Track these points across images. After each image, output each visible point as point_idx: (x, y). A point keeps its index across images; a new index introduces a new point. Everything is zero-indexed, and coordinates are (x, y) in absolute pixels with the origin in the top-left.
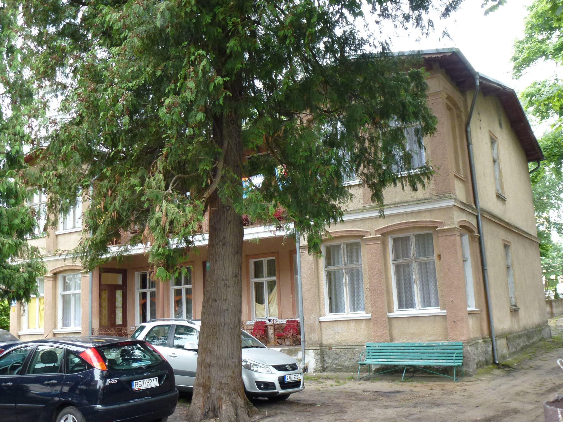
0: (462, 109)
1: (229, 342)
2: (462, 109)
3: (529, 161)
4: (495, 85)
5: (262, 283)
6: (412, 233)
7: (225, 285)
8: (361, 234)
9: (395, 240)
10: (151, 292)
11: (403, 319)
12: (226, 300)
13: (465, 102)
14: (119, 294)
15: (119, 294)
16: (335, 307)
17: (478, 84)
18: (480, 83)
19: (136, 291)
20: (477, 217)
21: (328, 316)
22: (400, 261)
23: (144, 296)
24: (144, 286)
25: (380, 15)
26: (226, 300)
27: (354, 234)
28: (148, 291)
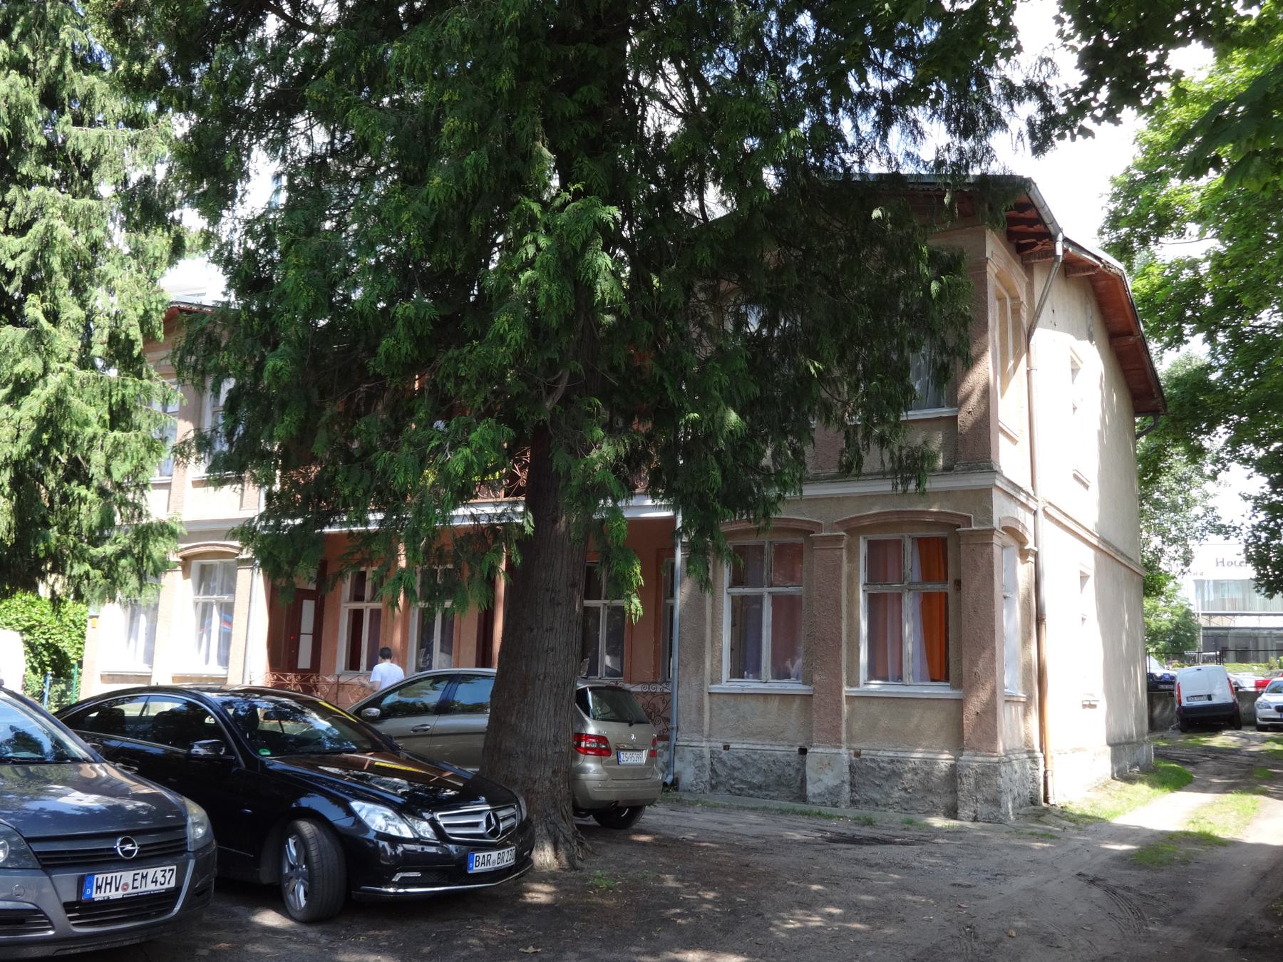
0: (1023, 298)
1: (552, 713)
2: (1023, 298)
3: (1137, 413)
4: (1090, 258)
5: (596, 611)
6: (906, 535)
7: (552, 600)
8: (806, 527)
9: (872, 545)
10: (372, 611)
11: (876, 702)
12: (551, 629)
13: (1030, 285)
14: (308, 607)
15: (308, 607)
16: (744, 663)
17: (1059, 252)
18: (1065, 251)
19: (343, 605)
20: (1035, 513)
21: (728, 684)
22: (879, 589)
23: (357, 616)
24: (358, 597)
25: (88, 488)
26: (551, 629)
27: (792, 525)
28: (366, 606)
